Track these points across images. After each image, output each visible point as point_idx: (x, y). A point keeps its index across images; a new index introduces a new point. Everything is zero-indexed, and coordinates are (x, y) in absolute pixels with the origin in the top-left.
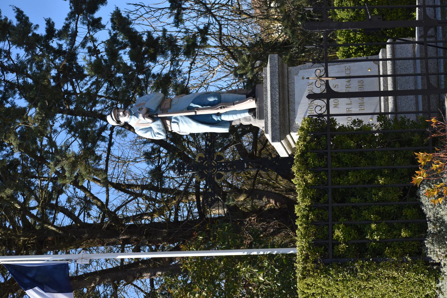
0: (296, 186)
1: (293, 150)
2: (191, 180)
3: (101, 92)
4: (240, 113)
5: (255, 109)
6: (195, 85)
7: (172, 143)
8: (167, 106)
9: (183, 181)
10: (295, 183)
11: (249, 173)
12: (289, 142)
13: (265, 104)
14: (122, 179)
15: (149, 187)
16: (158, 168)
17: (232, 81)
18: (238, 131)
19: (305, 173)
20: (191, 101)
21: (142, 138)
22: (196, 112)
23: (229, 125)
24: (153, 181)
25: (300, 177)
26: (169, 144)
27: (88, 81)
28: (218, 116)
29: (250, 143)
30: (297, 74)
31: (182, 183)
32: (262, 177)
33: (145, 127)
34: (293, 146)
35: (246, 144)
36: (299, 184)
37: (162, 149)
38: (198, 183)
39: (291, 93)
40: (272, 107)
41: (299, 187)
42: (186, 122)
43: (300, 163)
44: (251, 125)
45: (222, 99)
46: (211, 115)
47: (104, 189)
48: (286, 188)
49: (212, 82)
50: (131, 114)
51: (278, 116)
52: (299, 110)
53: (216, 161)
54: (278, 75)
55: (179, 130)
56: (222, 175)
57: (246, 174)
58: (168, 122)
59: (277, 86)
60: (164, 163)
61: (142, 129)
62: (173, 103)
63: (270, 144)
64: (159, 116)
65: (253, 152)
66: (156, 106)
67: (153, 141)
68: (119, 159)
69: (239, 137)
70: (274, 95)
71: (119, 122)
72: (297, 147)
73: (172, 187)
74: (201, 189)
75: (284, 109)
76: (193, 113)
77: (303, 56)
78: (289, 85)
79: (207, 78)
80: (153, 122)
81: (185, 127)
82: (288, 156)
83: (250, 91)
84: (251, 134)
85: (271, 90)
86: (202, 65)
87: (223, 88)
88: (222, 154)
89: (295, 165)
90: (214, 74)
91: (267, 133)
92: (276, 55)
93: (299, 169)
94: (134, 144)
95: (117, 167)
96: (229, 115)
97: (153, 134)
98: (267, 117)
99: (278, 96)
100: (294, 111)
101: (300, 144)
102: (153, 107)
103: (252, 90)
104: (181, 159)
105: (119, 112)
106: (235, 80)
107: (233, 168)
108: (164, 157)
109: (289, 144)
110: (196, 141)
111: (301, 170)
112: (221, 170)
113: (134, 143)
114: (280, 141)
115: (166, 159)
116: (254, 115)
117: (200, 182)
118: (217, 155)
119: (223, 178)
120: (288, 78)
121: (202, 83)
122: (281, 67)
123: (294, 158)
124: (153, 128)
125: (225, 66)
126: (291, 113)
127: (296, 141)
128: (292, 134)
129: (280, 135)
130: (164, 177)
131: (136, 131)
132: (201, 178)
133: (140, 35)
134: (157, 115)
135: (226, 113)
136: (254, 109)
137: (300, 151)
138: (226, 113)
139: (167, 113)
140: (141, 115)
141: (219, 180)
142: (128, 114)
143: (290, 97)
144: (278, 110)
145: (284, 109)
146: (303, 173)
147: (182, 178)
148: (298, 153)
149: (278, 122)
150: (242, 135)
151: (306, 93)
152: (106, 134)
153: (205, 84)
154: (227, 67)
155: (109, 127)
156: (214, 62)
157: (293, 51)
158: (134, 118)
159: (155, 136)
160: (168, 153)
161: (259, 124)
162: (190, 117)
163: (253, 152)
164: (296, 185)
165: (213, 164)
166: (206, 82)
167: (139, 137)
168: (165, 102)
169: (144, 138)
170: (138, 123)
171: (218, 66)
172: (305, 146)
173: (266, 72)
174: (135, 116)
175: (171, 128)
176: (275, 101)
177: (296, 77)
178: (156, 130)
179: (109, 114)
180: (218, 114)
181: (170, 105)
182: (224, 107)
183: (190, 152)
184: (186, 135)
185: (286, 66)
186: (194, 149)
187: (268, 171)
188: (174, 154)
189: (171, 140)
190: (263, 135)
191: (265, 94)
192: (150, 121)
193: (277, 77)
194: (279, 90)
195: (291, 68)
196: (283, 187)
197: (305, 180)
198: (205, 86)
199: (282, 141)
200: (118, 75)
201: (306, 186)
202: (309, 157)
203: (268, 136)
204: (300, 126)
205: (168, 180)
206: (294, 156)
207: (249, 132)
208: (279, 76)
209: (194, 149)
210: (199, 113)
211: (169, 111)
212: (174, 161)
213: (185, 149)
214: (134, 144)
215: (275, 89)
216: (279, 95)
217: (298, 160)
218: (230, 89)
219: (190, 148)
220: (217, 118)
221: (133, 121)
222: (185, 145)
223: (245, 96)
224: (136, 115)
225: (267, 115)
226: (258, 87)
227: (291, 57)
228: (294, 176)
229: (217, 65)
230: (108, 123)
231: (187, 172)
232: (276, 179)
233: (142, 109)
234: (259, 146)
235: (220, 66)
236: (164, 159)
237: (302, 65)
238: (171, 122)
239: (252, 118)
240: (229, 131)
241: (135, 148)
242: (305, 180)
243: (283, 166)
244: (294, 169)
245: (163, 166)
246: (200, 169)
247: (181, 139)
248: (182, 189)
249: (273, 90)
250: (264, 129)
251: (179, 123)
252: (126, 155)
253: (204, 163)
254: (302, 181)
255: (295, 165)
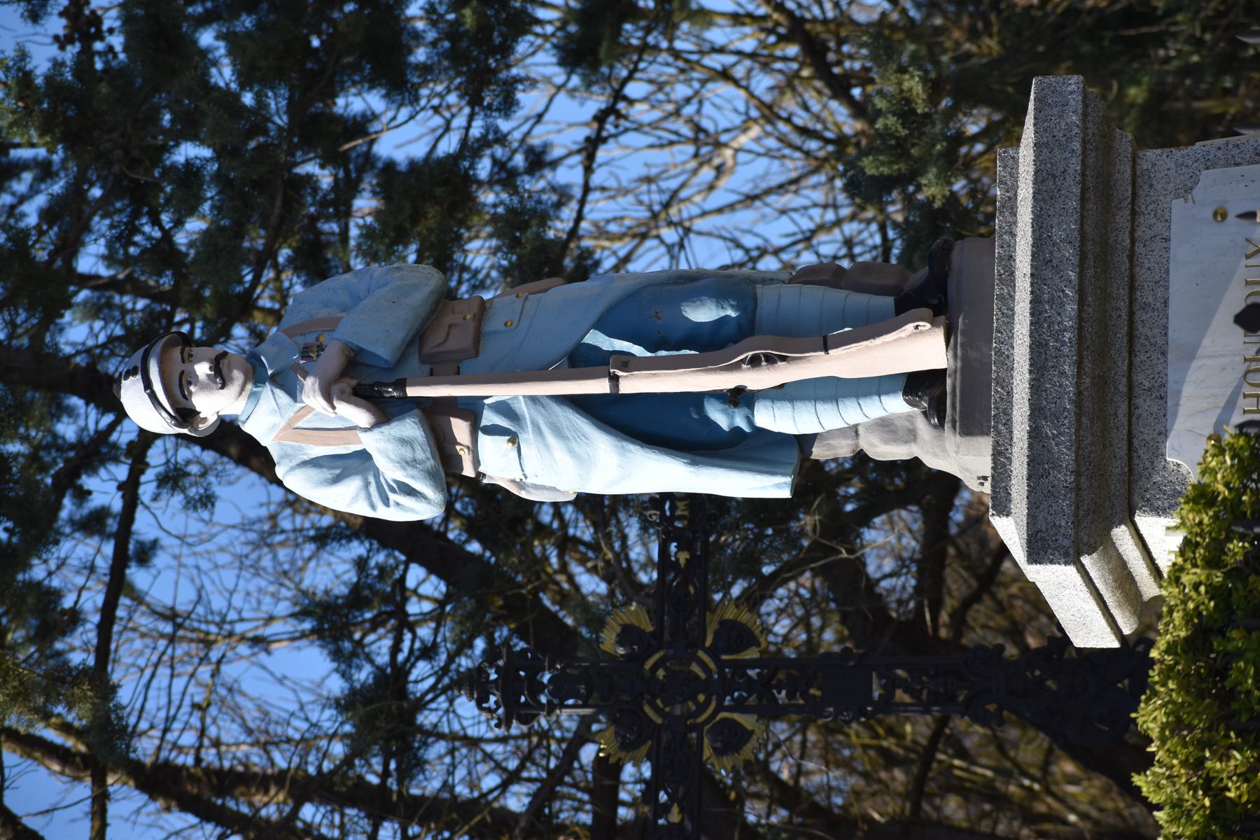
0: (1160, 815)
1: (1148, 611)
2: (571, 753)
3: (90, 260)
4: (856, 395)
5: (938, 375)
6: (613, 228)
7: (475, 547)
8: (459, 340)
9: (527, 759)
10: (1154, 799)
11: (891, 732)
12: (1123, 565)
13: (999, 352)
14: (189, 739)
15: (333, 788)
16: (393, 679)
17: (816, 212)
18: (841, 492)
19: (1209, 744)
20: (594, 314)
21: (310, 507)
22: (615, 380)
23: (794, 456)
24: (358, 749)
25: (1184, 764)
26: (457, 550)
27: (23, 199)
28: (736, 405)
29: (902, 563)
30: (1186, 191)
31: (522, 767)
32: (962, 753)
33: (333, 453)
34: (1149, 588)
35: (877, 565)
36: (1176, 804)
37: (415, 574)
38: (608, 770)
39: (1145, 296)
40: (1038, 368)
41: (1172, 821)
42: (558, 432)
43: (1184, 687)
44: (916, 462)
45: (762, 316)
46: (696, 399)
47: (84, 790)
48: (1096, 823)
49: (704, 214)
50: (256, 375)
51: (1068, 422)
52: (1187, 390)
53: (713, 652)
54: (1076, 190)
55: (518, 476)
56: (747, 735)
57: (876, 736)
58: (460, 429)
59: (1069, 252)
60: (428, 652)
61: (315, 463)
62: (494, 323)
63: (1020, 575)
64: (412, 392)
65: (919, 611)
66: (399, 335)
67: (373, 530)
68: (178, 626)
69: (842, 529)
70: (1051, 302)
71: (185, 415)
72: (1170, 593)
73: (462, 790)
74: (624, 804)
75: (1102, 383)
76: (600, 387)
77: (1227, 92)
78: (1139, 249)
79: (684, 194)
80: (377, 424)
81: (553, 459)
82: (1116, 644)
83: (920, 274)
84: (909, 517)
85: (1036, 276)
86: (657, 114)
87: (763, 252)
88: (745, 617)
89: (1155, 694)
90: (720, 170)
91: (1003, 508)
92: (1074, 82)
93: (1179, 720)
94: (264, 541)
95: (164, 672)
96: (799, 405)
97: (373, 489)
98: (1008, 424)
99: (1071, 308)
100: (1162, 395)
101: (1185, 579)
102: (380, 335)
103: (931, 273)
104: (522, 633)
105: (189, 359)
106: (835, 207)
107: (805, 695)
108: (424, 618)
109: (1124, 579)
110: (608, 537)
111: (1191, 728)
112: (739, 706)
113: (266, 534)
114: (1072, 557)
115: (436, 631)
116: (937, 412)
117: (619, 768)
118: (723, 623)
119: (747, 751)
120: (1134, 214)
121: (655, 216)
122: (1098, 147)
123: (1154, 654)
124: (379, 461)
125: (782, 127)
126: (1145, 405)
127: (1165, 561)
128: (1144, 522)
129: (1077, 523)
130: (420, 729)
131: (280, 472)
132: (629, 747)
133: (199, 169)
134: (401, 384)
135: (782, 393)
136: (937, 376)
137: (1188, 618)
138: (782, 393)
139: (457, 377)
140: (310, 384)
141: (728, 761)
142: (238, 376)
143: (1140, 315)
144: (1069, 386)
145: (1102, 383)
146: (1202, 745)
147: (524, 744)
148: (1174, 629)
149: (1067, 456)
150: (864, 518)
151: (1235, 300)
152: (103, 488)
153: (670, 224)
154: (796, 139)
155: (123, 437)
156: (723, 106)
157: (1168, 60)
158: (271, 398)
159: (386, 502)
160: (448, 598)
161: (964, 459)
162: (580, 404)
163: (919, 611)
164: (1159, 807)
165: (695, 668)
166: (673, 211)
167: (295, 503)
168: (450, 319)
169: (323, 510)
170: (292, 429)
171: (744, 129)
172: (1213, 592)
173: (1014, 176)
174: (282, 387)
175: (476, 462)
176: (1057, 335)
177: (1177, 205)
178: (391, 472)
179: (131, 372)
180: (739, 398)
181: (478, 337)
182: (771, 360)
183: (572, 597)
184: (556, 506)
185: (1125, 139)
186: (591, 584)
187: (1002, 722)
188: (482, 605)
189: (473, 529)
190: (977, 521)
191: (1001, 298)
192: (358, 416)
193: (1074, 203)
194: (1081, 276)
195: (1151, 154)
196: (1084, 816)
197: (1210, 785)
198: (670, 235)
199: (1086, 560)
200: (188, 152)
201: (1213, 816)
202: (1239, 654)
203: (1010, 530)
204: (1193, 478)
205: (441, 747)
206: (1151, 644)
207: (903, 504)
208: (1083, 200)
209: (591, 584)
210: (632, 384)
211: (467, 366)
212: (480, 644)
213: (548, 582)
214: (264, 541)
215: (1057, 269)
216: (1081, 302)
217: (1171, 668)
218: (808, 258)
219: (571, 579)
220: (732, 417)
221: (265, 416)
222: (546, 559)
223: (888, 301)
224: (287, 383)
225: (1007, 413)
226: (963, 254)
227: (1159, 95)
228: (1149, 760)
229: (738, 120)
230: (125, 415)
231: (551, 708)
232: (1045, 767)
233: (321, 348)
234: (957, 582)
235: (755, 131)
236: (425, 632)
237: (1220, 142)
238: (475, 429)
239: (922, 425)
240: (796, 489)
241: (267, 562)
242: (1210, 785)
243: (1086, 699)
244: (1150, 717)
245: (422, 668)
246: (617, 693)
247: (523, 522)
248: (517, 800)
249: (1048, 273)
250: (987, 488)
251: (523, 438)
252: (218, 603)
253: (649, 664)
254: (1192, 787)
255: (1155, 694)
